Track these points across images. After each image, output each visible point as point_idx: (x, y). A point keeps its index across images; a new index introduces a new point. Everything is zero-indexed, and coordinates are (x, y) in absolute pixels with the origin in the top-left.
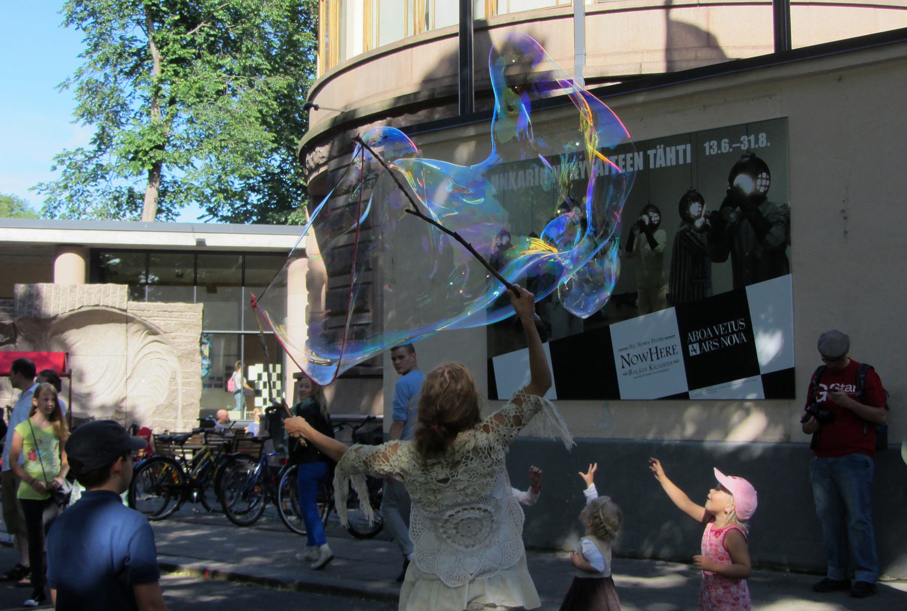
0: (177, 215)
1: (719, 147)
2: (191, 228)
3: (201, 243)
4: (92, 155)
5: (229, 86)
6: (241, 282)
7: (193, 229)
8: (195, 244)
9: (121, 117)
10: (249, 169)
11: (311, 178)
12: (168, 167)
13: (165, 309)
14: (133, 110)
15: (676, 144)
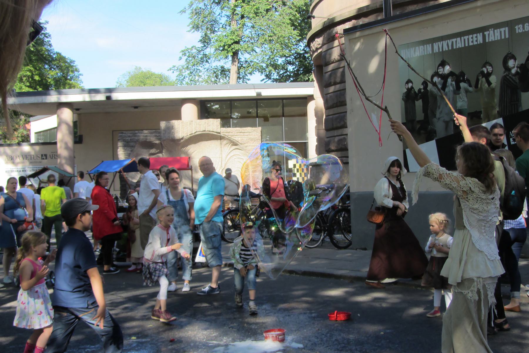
0: (249, 80)
1: (523, 28)
2: (254, 87)
3: (259, 94)
4: (201, 49)
5: (273, 6)
6: (282, 114)
7: (254, 87)
8: (255, 95)
9: (215, 28)
10: (286, 52)
11: (314, 56)
12: (242, 53)
13: (241, 131)
14: (221, 23)
15: (500, 28)
